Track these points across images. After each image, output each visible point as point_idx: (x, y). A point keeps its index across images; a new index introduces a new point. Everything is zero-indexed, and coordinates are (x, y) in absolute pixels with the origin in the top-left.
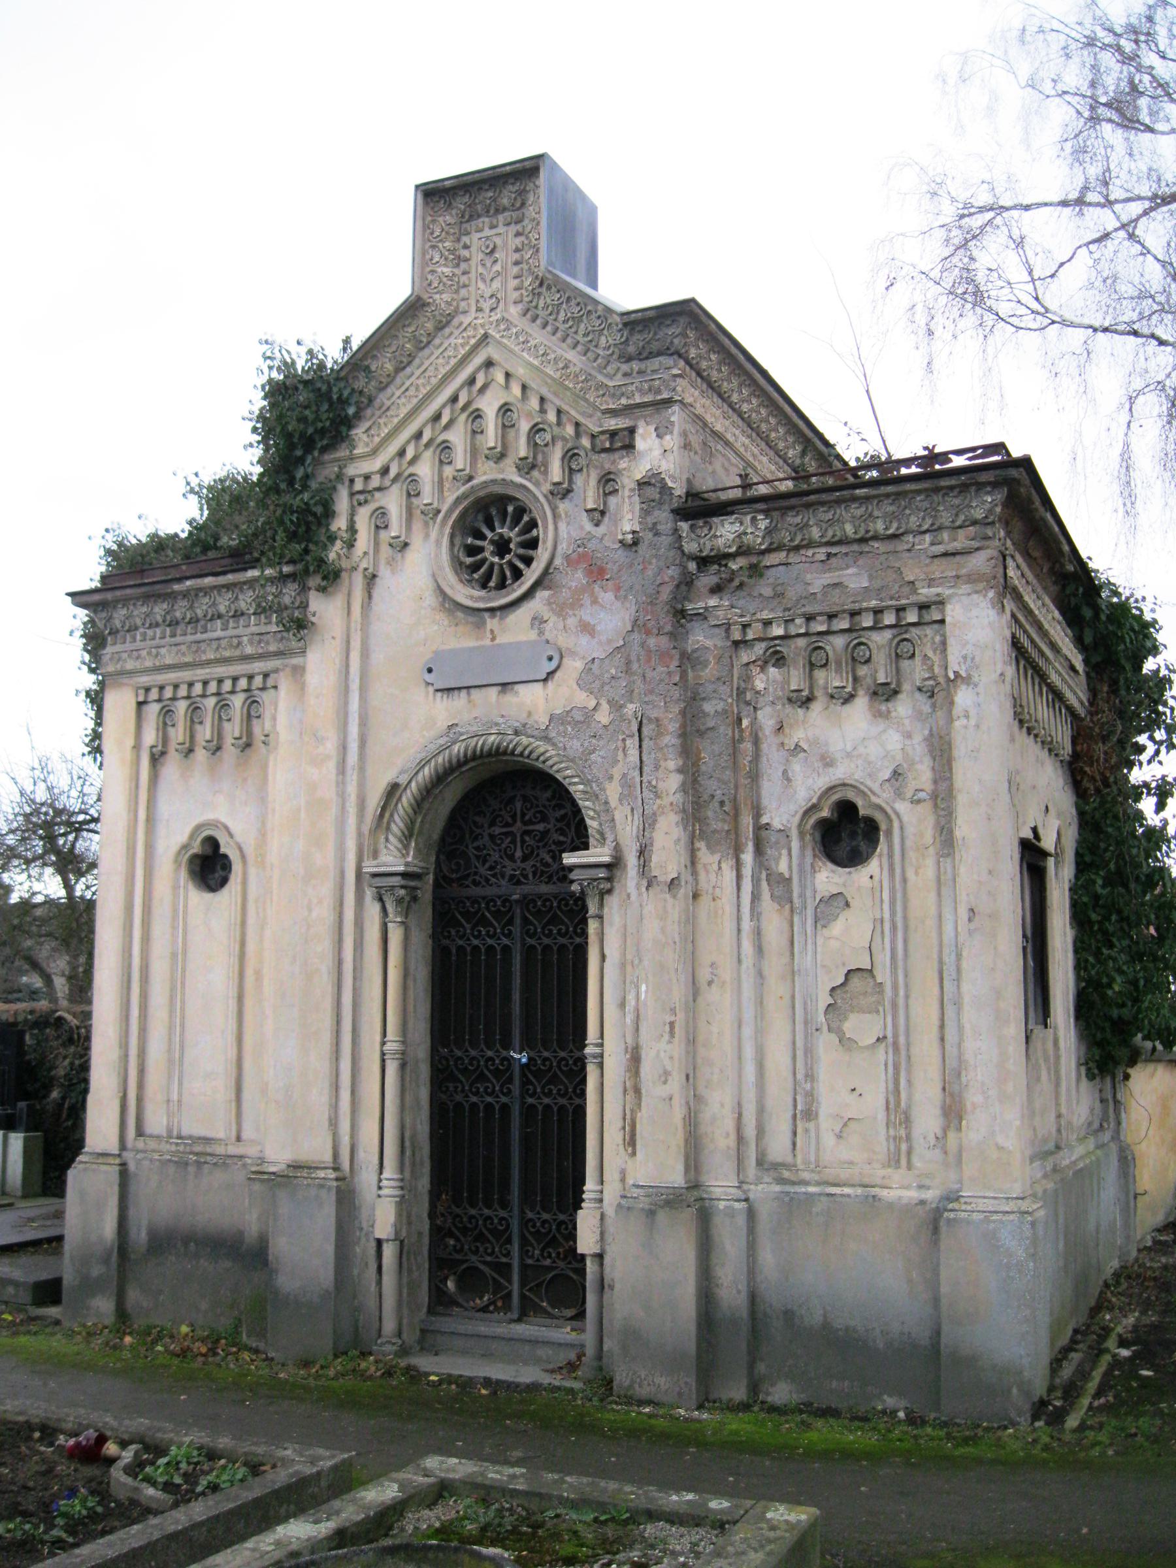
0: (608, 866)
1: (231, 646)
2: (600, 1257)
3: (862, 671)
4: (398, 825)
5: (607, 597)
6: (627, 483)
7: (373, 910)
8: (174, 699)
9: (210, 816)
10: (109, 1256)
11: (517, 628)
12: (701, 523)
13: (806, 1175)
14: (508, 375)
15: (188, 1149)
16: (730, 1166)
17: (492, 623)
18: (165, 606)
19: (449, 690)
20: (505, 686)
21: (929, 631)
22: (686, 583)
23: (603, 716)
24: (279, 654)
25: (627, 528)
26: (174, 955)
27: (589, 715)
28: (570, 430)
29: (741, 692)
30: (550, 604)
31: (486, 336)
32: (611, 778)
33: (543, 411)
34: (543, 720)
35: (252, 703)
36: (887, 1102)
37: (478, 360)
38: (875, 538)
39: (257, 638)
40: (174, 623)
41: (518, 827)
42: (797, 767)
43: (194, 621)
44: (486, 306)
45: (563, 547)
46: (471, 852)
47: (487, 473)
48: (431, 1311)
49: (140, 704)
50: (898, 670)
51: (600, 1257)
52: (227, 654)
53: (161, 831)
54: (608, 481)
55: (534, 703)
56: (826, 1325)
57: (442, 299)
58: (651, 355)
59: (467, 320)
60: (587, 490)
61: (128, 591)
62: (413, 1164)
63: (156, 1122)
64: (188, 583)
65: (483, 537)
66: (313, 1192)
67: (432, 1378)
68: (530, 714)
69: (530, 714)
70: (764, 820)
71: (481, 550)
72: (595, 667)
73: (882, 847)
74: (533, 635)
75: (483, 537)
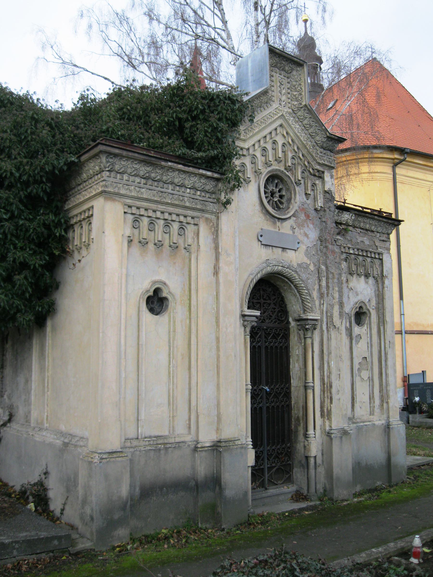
1: (179, 200)
5: (311, 226)
9: (157, 278)
10: (125, 506)
11: (286, 228)
12: (341, 211)
13: (358, 420)
15: (155, 443)
17: (278, 224)
18: (148, 169)
19: (266, 245)
20: (284, 249)
23: (312, 267)
24: (202, 211)
25: (320, 205)
27: (308, 266)
30: (295, 223)
32: (314, 289)
34: (295, 265)
36: (370, 396)
39: (192, 200)
42: (351, 294)
47: (275, 166)
52: (177, 202)
56: (366, 465)
61: (136, 155)
64: (170, 164)
66: (239, 450)
67: (287, 514)
68: (291, 261)
69: (291, 261)
72: (309, 249)
74: (291, 233)
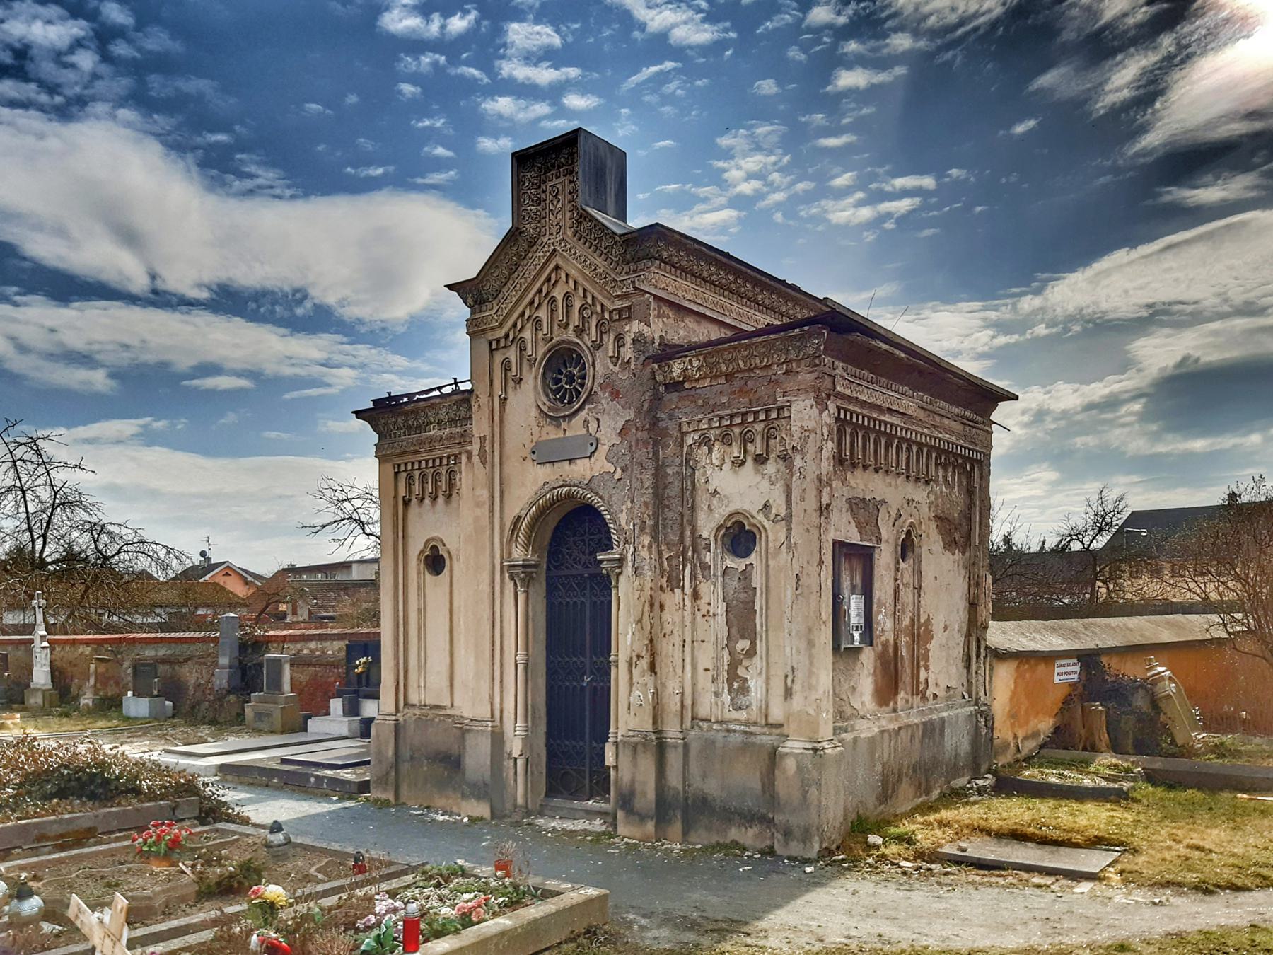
0: (618, 560)
2: (616, 767)
3: (750, 447)
4: (522, 538)
6: (628, 340)
7: (510, 585)
8: (412, 469)
11: (575, 428)
14: (567, 275)
16: (677, 721)
17: (564, 425)
21: (784, 421)
22: (657, 399)
26: (419, 610)
28: (599, 308)
29: (687, 461)
31: (554, 250)
33: (585, 296)
35: (451, 473)
37: (552, 266)
38: (756, 368)
40: (409, 428)
41: (586, 537)
43: (419, 427)
44: (554, 231)
45: (599, 380)
46: (564, 550)
48: (546, 795)
49: (396, 474)
50: (768, 445)
51: (616, 767)
53: (411, 542)
54: (619, 338)
55: (581, 470)
57: (530, 228)
58: (640, 259)
59: (545, 240)
60: (609, 341)
62: (533, 718)
63: (414, 698)
65: (561, 373)
70: (697, 534)
71: (560, 380)
73: (757, 548)
74: (584, 431)
75: (561, 373)
